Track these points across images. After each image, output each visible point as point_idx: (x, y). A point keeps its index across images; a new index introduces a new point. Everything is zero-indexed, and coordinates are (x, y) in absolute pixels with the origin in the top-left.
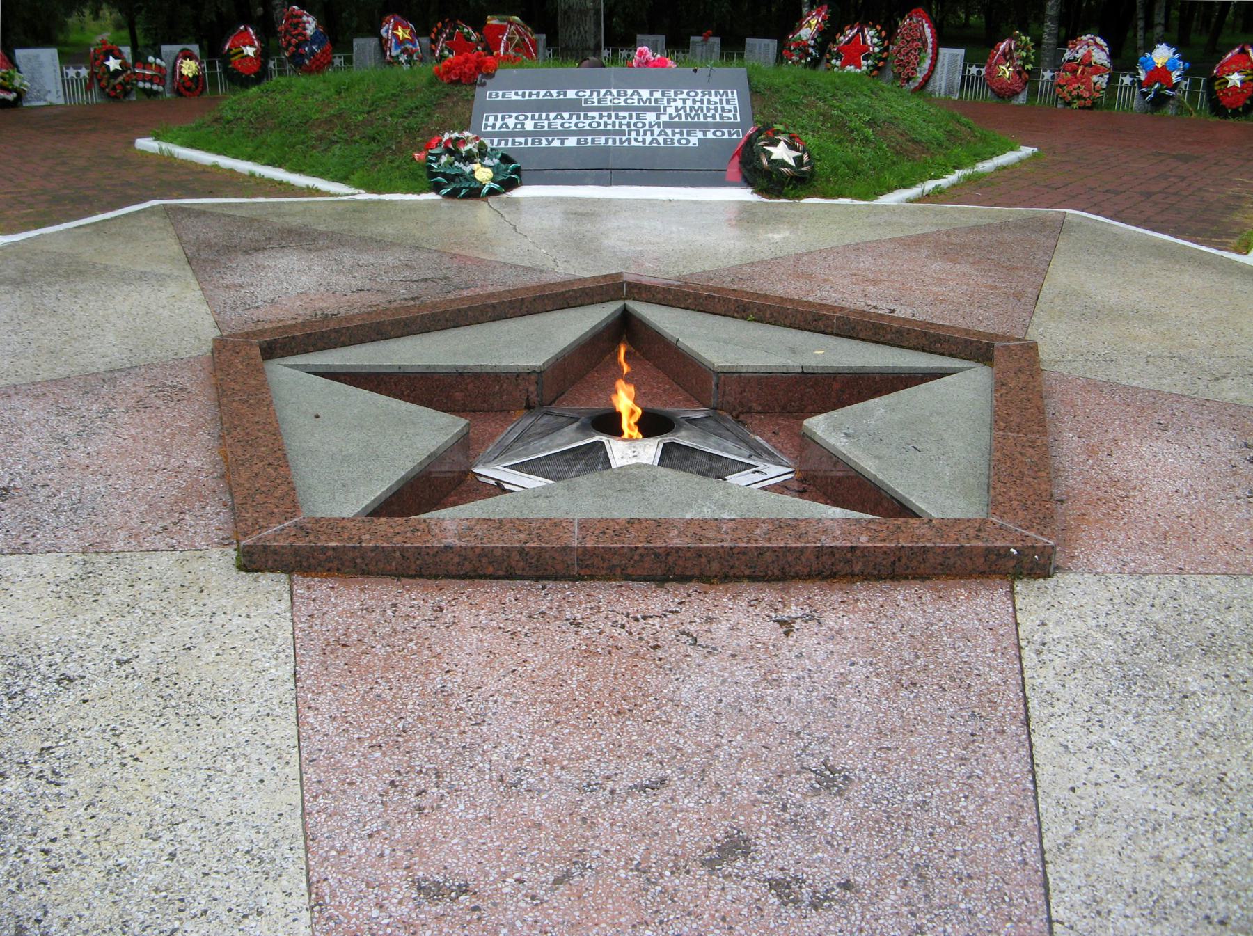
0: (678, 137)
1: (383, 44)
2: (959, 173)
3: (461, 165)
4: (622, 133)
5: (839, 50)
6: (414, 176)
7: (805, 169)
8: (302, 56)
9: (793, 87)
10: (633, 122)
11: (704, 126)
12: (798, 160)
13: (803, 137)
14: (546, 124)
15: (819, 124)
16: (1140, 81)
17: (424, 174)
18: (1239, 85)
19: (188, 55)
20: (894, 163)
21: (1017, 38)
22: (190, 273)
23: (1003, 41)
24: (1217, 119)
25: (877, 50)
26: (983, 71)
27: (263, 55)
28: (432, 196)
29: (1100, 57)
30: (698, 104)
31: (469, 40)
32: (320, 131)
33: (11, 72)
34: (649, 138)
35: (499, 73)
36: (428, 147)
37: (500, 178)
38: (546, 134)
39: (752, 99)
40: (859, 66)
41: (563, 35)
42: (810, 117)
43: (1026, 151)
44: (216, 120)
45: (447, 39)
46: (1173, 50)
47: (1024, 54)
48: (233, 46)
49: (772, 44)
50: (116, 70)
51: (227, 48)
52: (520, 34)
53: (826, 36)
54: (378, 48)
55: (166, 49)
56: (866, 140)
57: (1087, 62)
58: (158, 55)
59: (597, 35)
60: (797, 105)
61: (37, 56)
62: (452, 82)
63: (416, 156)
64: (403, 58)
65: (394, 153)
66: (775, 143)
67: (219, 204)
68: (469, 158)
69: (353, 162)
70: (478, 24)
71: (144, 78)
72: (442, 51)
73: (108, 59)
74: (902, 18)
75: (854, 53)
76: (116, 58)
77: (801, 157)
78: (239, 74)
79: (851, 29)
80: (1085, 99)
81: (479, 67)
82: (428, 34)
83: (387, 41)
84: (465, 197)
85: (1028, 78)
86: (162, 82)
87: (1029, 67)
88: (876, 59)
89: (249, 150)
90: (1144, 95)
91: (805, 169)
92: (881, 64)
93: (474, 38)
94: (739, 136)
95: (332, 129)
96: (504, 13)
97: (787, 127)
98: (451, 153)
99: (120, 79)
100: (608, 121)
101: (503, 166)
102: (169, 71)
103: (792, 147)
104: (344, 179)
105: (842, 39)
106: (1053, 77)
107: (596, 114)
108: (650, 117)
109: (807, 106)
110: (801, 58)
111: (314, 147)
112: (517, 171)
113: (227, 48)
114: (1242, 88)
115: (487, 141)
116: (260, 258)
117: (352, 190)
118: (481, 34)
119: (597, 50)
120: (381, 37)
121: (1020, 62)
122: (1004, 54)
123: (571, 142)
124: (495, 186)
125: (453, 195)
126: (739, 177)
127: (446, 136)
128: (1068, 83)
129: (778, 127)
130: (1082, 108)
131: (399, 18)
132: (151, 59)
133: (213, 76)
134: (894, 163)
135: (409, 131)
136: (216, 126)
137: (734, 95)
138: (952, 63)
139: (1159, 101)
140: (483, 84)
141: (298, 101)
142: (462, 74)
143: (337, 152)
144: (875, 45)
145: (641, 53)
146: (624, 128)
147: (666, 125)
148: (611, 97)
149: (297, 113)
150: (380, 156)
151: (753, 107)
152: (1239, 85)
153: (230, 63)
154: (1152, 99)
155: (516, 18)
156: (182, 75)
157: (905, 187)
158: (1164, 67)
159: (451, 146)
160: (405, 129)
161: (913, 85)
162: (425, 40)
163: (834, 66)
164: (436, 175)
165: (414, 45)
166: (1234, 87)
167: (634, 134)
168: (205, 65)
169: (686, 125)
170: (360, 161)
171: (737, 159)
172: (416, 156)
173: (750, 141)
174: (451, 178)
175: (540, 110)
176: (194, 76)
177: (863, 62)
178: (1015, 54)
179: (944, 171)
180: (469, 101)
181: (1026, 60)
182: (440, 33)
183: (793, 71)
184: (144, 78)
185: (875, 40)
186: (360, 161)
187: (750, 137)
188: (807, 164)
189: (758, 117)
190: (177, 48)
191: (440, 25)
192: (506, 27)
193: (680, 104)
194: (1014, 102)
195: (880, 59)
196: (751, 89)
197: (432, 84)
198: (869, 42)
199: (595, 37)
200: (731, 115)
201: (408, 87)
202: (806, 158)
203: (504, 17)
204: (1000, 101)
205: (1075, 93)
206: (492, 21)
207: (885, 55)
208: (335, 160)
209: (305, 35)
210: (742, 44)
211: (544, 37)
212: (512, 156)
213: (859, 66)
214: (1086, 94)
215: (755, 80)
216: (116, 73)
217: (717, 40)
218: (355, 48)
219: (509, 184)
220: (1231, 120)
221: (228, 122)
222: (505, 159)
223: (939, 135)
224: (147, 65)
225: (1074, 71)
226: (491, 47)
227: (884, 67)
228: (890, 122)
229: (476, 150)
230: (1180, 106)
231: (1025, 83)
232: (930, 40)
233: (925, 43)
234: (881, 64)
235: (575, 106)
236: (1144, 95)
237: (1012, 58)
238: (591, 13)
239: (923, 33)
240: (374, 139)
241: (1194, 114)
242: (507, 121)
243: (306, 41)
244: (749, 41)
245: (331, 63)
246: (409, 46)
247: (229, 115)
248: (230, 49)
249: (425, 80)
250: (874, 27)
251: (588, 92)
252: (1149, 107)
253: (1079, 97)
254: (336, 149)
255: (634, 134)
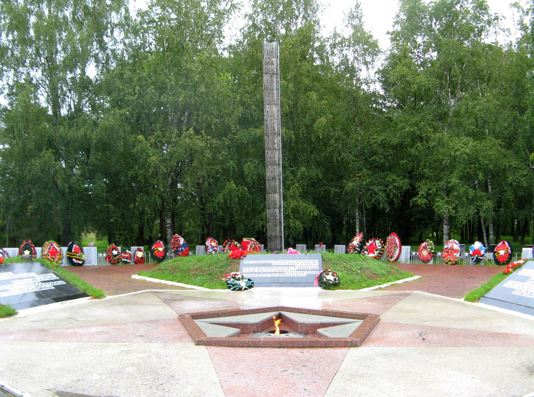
0: (300, 273)
1: (206, 248)
2: (390, 283)
3: (236, 281)
4: (284, 273)
5: (367, 248)
6: (223, 284)
7: (337, 282)
8: (178, 251)
9: (336, 259)
10: (287, 269)
11: (308, 270)
12: (335, 279)
13: (338, 273)
14: (261, 270)
15: (343, 269)
16: (471, 254)
17: (226, 284)
18: (503, 254)
19: (140, 250)
20: (366, 280)
21: (428, 242)
22: (166, 305)
23: (423, 243)
24: (498, 266)
25: (380, 247)
26: (417, 253)
27: (166, 250)
28: (228, 290)
29: (456, 246)
30: (306, 264)
31: (237, 246)
32: (193, 273)
33: (82, 254)
34: (291, 274)
35: (248, 256)
36: (227, 276)
37: (248, 285)
38: (262, 273)
39: (322, 263)
40: (374, 253)
41: (269, 244)
42: (340, 267)
43: (416, 277)
44: (159, 269)
45: (229, 246)
46: (481, 243)
47: (430, 247)
48: (155, 247)
49: (344, 247)
50: (116, 255)
51: (153, 248)
52: (255, 244)
53: (362, 243)
54: (205, 249)
55: (132, 248)
56: (358, 274)
57: (452, 249)
58: (130, 250)
59: (281, 244)
60: (336, 264)
61: (90, 249)
62: (234, 258)
63: (223, 279)
64: (213, 252)
65: (217, 278)
66: (328, 274)
67: (162, 289)
68: (239, 279)
69: (204, 281)
70: (240, 240)
71: (124, 257)
72: (227, 250)
73: (113, 251)
74: (388, 236)
75: (371, 249)
76: (116, 250)
77: (336, 279)
78: (157, 257)
79: (371, 240)
80: (452, 261)
81: (242, 254)
82: (222, 245)
83: (208, 246)
84: (237, 290)
85: (433, 255)
86: (130, 259)
87: (433, 251)
88: (380, 250)
89: (171, 278)
90: (473, 259)
91: (337, 282)
92: (382, 252)
93: (238, 245)
94: (318, 273)
95: (197, 272)
96: (249, 237)
97: (332, 270)
98: (233, 278)
99: (117, 257)
100: (280, 269)
101: (249, 282)
102: (133, 255)
103: (333, 276)
104: (202, 286)
105: (368, 244)
106: (441, 255)
107: (276, 267)
108: (292, 268)
109: (340, 264)
110: (354, 251)
111: (192, 277)
112: (253, 283)
113: (153, 248)
114: (505, 255)
115: (244, 275)
116: (183, 302)
117: (205, 288)
118: (241, 244)
119: (281, 249)
120: (206, 245)
121: (430, 250)
122: (424, 247)
123: (269, 275)
124: (247, 287)
125: (234, 289)
126: (317, 285)
127: (232, 273)
128: (446, 256)
129: (329, 270)
130: (452, 264)
131: (212, 239)
132: (127, 251)
133: (147, 258)
134: (366, 280)
135: (221, 272)
136: (159, 271)
137: (317, 262)
138: (406, 251)
139: (478, 261)
140: (243, 259)
141: (186, 264)
142: (237, 256)
143: (199, 278)
144: (379, 246)
145: (290, 250)
146: (284, 271)
147: (297, 270)
148: (280, 262)
149: (186, 267)
150: (212, 279)
151: (323, 265)
152: (503, 254)
153: (154, 253)
154: (475, 260)
155: (253, 239)
156: (137, 257)
157: (368, 287)
158: (478, 249)
159: (233, 276)
160: (220, 272)
161: (393, 259)
162: (221, 246)
163: (365, 254)
164: (229, 284)
165: (217, 248)
166: (502, 255)
167: (287, 273)
168: (145, 254)
169: (303, 270)
170: (206, 281)
171: (317, 279)
172: (223, 279)
173: (321, 274)
174: (233, 285)
175: (259, 266)
176: (142, 257)
177: (376, 252)
178: (428, 247)
179: (384, 282)
180: (239, 264)
181: (432, 249)
182: (226, 244)
183: (352, 255)
184: (124, 257)
185: (379, 244)
186: (206, 281)
187: (321, 273)
188: (338, 280)
189: (324, 267)
190: (136, 248)
191: (226, 241)
192: (249, 242)
193: (301, 264)
194: (429, 264)
195: (381, 251)
196: (322, 259)
197: (228, 259)
198: (377, 245)
199: (280, 245)
200: (316, 267)
201: (220, 260)
202: (337, 279)
203: (249, 239)
204: (424, 263)
205: (449, 259)
206: (245, 240)
207: (383, 249)
208: (198, 280)
209: (180, 244)
210: (333, 247)
211: (263, 245)
212: (251, 279)
213: (374, 253)
214: (453, 260)
215: (324, 258)
216: (116, 256)
217: (325, 246)
218: (197, 249)
219: (250, 287)
220: (502, 266)
221: (163, 270)
222: (249, 280)
223: (384, 272)
224: (126, 253)
225: (448, 252)
226: (245, 248)
227: (383, 253)
228: (367, 268)
229: (241, 277)
230: (485, 262)
231: (432, 257)
232: (398, 244)
233: (396, 245)
234: (382, 252)
235: (270, 265)
236: (473, 259)
237: (426, 248)
238: (279, 237)
239: (395, 241)
240: (210, 274)
241: (490, 265)
242: (250, 269)
243: (180, 246)
244: (335, 246)
245: (188, 254)
246: (216, 248)
247: (164, 268)
248: (154, 249)
249: (225, 258)
250: (379, 239)
251: (274, 261)
252: (475, 263)
253: (450, 261)
254: (199, 277)
255: (287, 273)
